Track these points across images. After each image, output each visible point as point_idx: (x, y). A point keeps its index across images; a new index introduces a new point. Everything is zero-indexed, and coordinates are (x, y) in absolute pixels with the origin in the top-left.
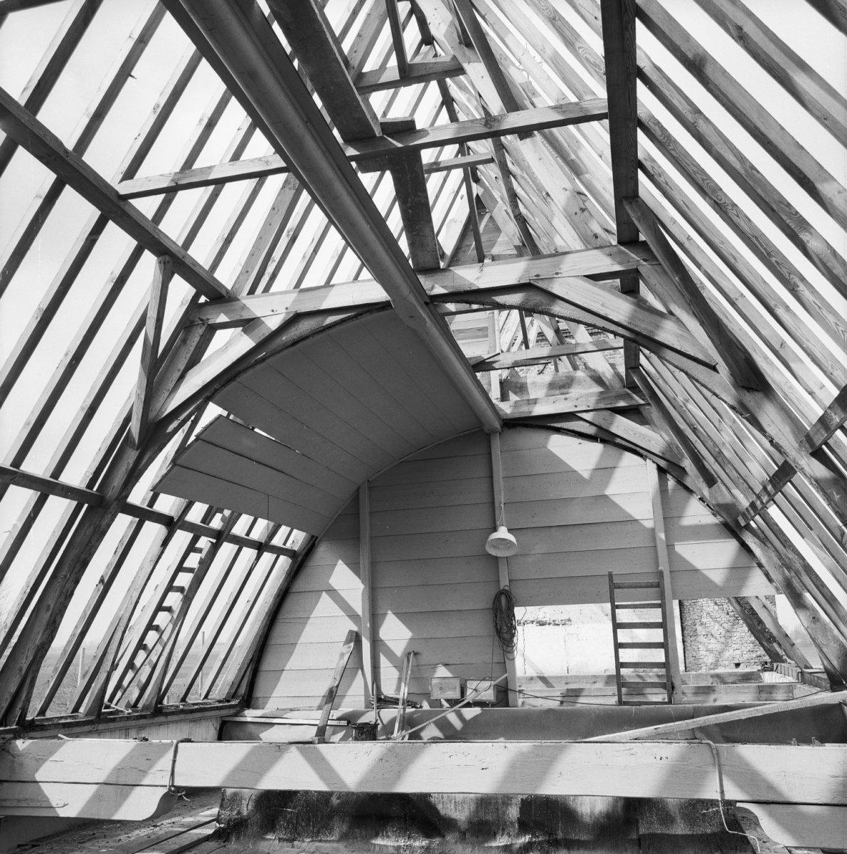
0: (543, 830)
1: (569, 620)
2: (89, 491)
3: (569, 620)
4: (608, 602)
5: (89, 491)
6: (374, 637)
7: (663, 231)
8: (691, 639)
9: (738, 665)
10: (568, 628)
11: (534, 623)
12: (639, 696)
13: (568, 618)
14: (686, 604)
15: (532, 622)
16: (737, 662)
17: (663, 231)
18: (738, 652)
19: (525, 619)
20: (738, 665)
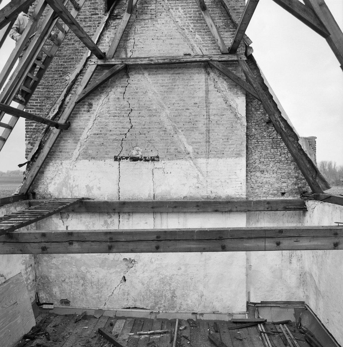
0: (39, 224)
1: (158, 157)
2: (52, 121)
3: (158, 157)
4: (18, 107)
5: (52, 121)
6: (5, 22)
7: (114, 4)
8: (251, 174)
9: (283, 194)
10: (157, 164)
11: (128, 159)
12: (250, 241)
13: (156, 155)
14: (250, 147)
15: (127, 158)
16: (283, 192)
17: (114, 4)
18: (285, 184)
19: (121, 155)
20: (283, 194)
